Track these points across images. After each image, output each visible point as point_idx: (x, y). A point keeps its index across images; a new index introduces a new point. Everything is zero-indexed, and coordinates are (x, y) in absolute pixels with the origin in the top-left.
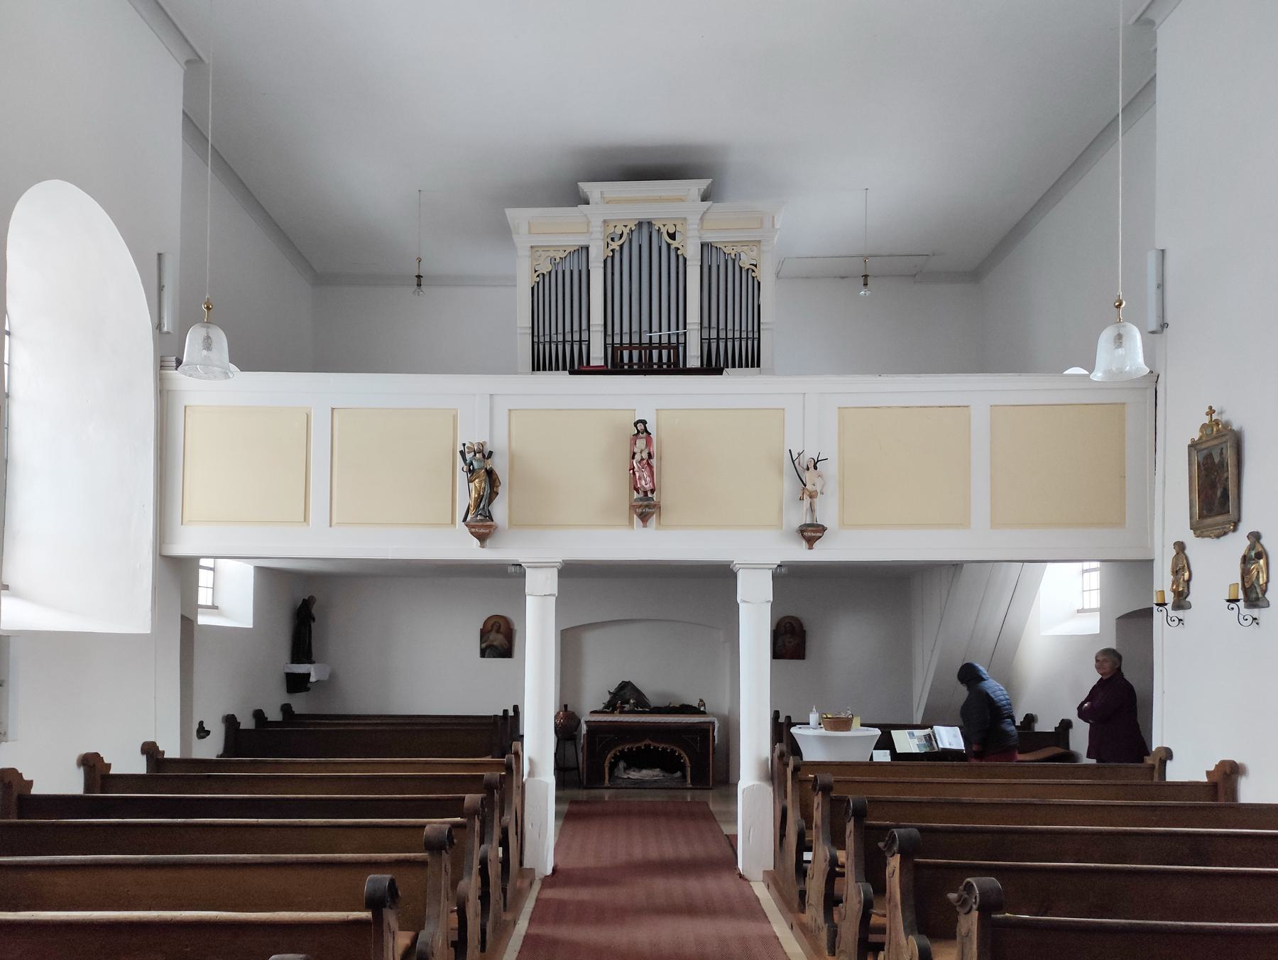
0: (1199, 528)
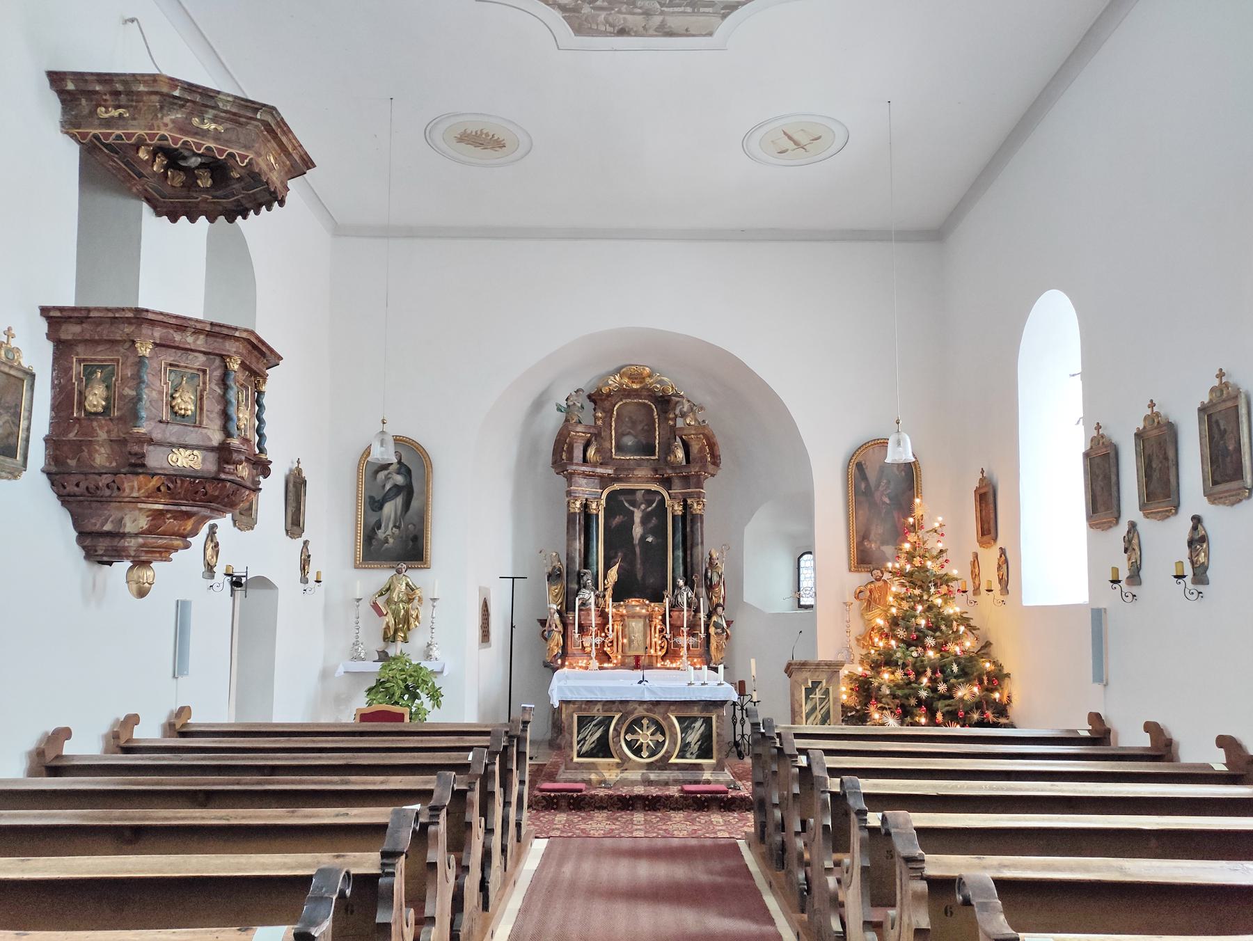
0: (982, 544)
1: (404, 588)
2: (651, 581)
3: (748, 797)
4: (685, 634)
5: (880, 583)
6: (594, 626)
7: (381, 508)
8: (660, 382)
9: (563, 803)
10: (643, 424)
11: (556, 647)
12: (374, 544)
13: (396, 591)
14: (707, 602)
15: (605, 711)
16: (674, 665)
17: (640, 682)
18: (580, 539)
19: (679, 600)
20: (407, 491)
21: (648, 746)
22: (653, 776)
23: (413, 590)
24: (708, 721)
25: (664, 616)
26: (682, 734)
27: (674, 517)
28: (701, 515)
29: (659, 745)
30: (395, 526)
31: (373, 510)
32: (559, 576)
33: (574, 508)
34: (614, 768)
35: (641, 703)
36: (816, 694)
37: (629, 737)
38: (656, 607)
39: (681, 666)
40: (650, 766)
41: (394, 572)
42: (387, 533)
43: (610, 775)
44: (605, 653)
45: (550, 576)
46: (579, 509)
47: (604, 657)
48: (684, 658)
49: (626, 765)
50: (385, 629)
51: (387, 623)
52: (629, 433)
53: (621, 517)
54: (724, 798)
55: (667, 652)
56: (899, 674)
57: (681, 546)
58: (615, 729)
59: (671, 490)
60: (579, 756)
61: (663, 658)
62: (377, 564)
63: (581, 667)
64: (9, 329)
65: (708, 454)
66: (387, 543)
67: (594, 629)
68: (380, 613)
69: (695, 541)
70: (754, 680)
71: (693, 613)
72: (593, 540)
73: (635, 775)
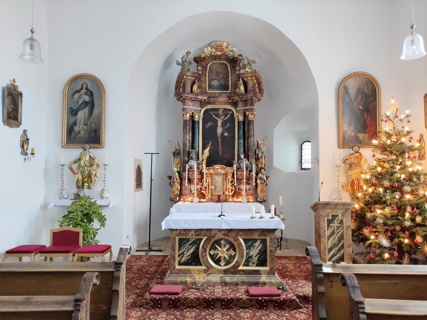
1: (88, 158)
2: (227, 156)
3: (294, 300)
4: (245, 183)
5: (357, 155)
6: (196, 179)
7: (76, 114)
8: (232, 51)
9: (165, 304)
10: (223, 74)
11: (176, 191)
12: (73, 134)
13: (83, 160)
14: (256, 166)
15: (196, 236)
16: (238, 200)
17: (220, 216)
18: (189, 134)
19: (241, 165)
20: (91, 105)
21: (225, 258)
22: (228, 279)
23: (93, 159)
24: (264, 242)
25: (233, 174)
26: (247, 250)
27: (239, 122)
28: (253, 121)
29: (232, 257)
30: (84, 124)
31: (72, 115)
32: (179, 153)
33: (186, 117)
34: (202, 272)
35: (220, 230)
36: (334, 223)
37: (212, 252)
38: (229, 169)
39: (242, 200)
40: (226, 272)
41: (82, 150)
42: (80, 128)
43: (200, 278)
44: (203, 194)
45: (174, 154)
46: (189, 118)
47: (202, 196)
48: (244, 196)
49: (210, 271)
50: (77, 181)
51: (78, 179)
52: (215, 79)
53: (211, 123)
54: (277, 300)
55: (234, 193)
56: (387, 210)
57: (242, 137)
58: (203, 247)
59: (237, 108)
60: (180, 264)
61: (233, 196)
62: (74, 145)
63: (189, 201)
64: (14, 79)
65: (257, 88)
66: (80, 134)
67: (196, 181)
68: (74, 173)
69: (250, 134)
70: (282, 208)
71: (249, 172)
72: (196, 135)
73: (215, 278)
